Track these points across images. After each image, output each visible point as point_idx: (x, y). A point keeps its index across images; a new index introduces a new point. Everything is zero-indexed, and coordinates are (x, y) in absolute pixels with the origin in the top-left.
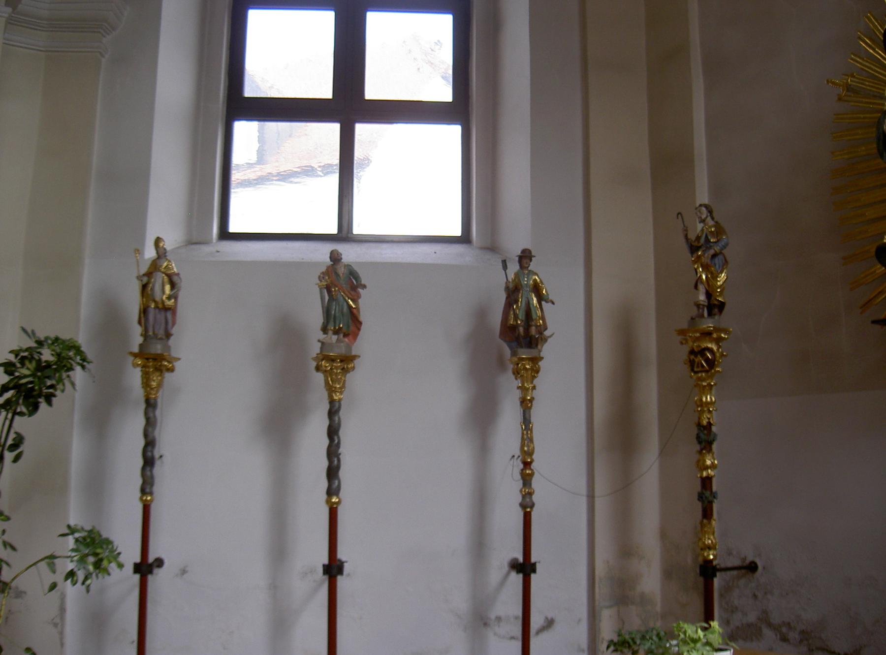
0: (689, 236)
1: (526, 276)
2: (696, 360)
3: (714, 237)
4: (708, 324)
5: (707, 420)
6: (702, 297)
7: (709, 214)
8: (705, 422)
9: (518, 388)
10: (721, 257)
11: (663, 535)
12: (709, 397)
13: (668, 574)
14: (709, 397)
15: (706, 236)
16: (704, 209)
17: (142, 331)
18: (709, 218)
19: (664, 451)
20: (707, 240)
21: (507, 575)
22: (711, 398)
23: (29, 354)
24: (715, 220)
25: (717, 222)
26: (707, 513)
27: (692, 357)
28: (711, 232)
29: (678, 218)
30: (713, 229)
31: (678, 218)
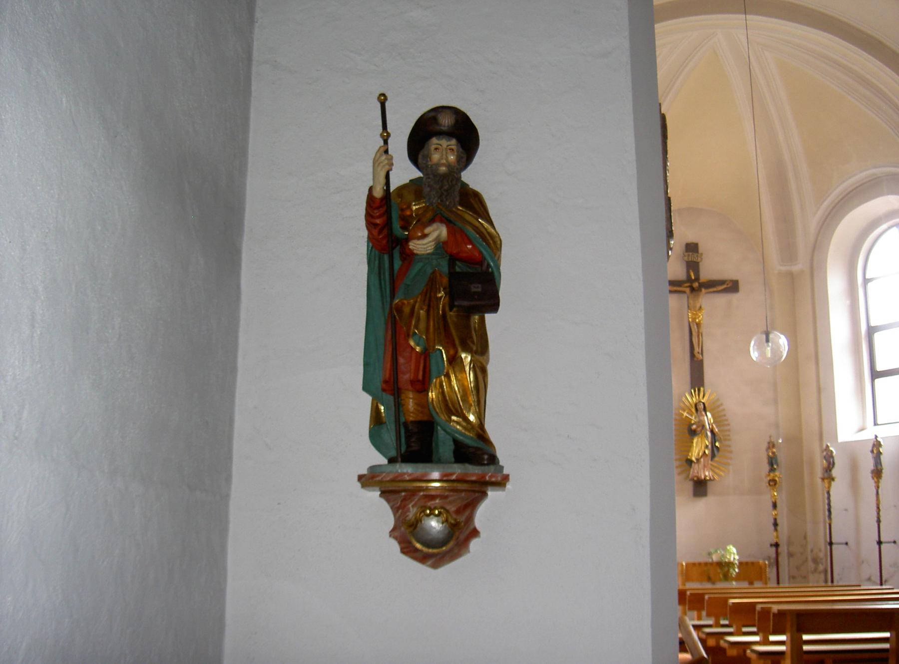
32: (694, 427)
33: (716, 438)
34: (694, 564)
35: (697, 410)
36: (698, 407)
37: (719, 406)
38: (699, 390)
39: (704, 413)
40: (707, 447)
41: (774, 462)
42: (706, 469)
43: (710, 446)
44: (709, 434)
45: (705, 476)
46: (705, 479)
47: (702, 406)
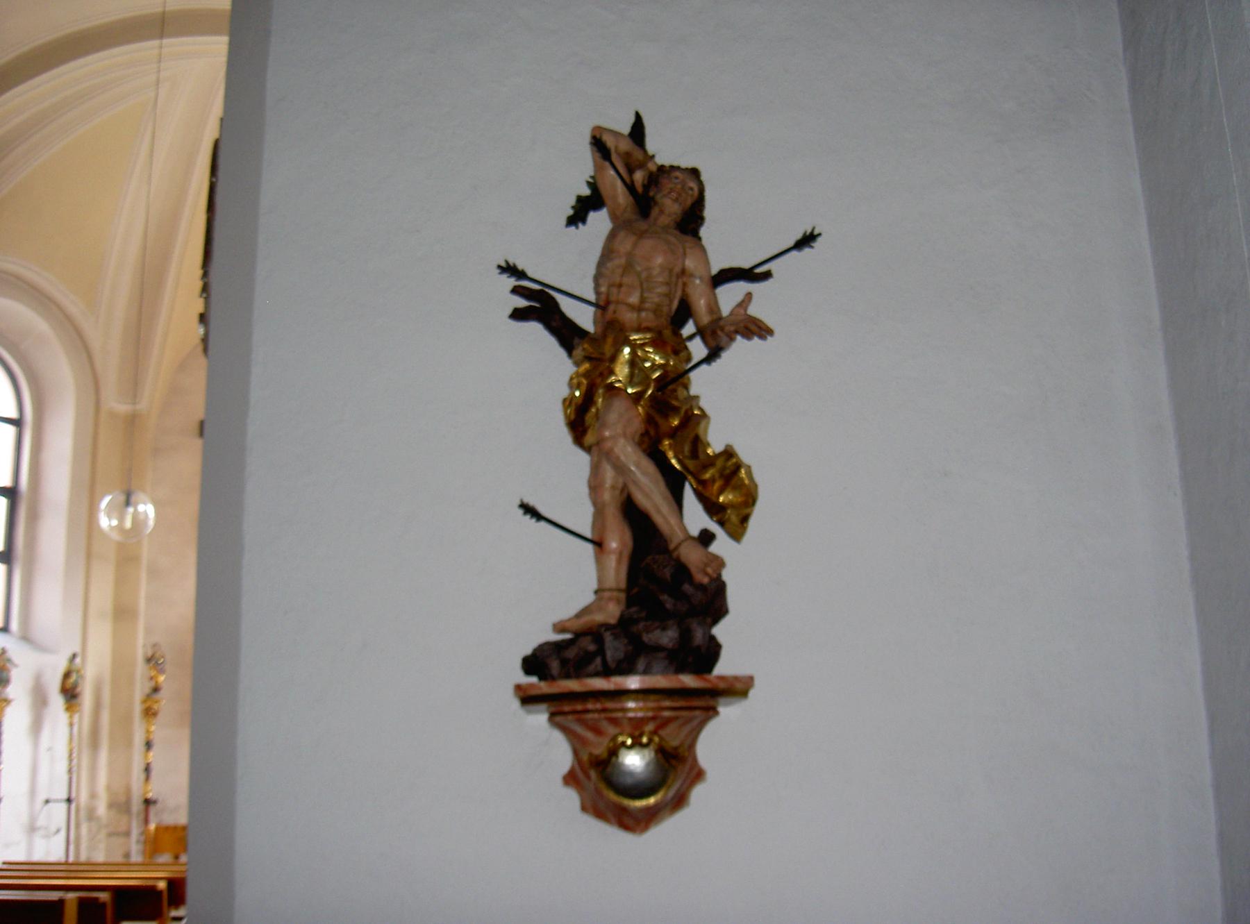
11: (109, 788)
13: (111, 805)
19: (112, 750)
21: (42, 808)
26: (147, 778)
34: (167, 828)
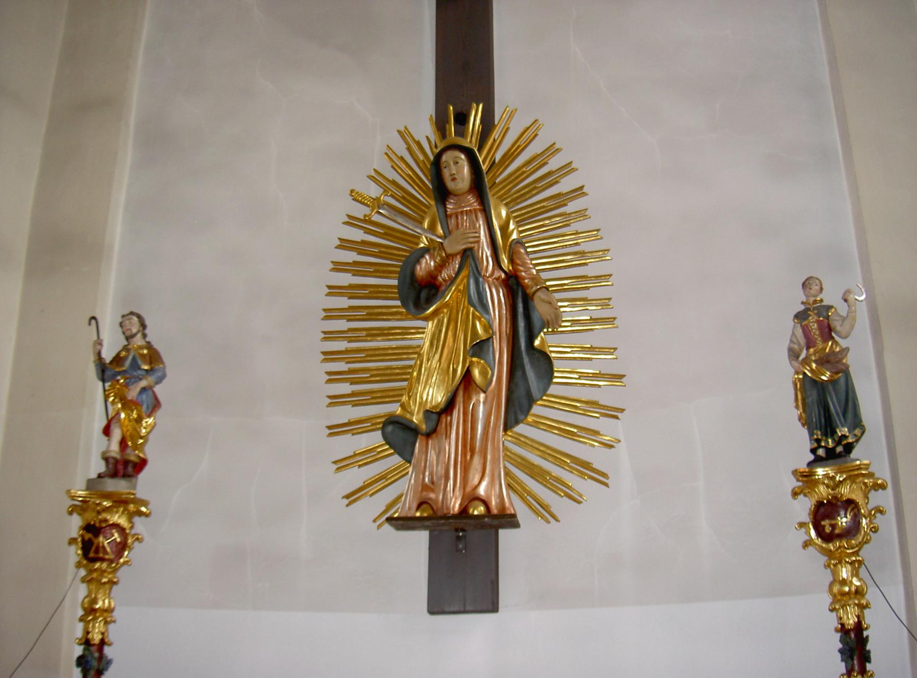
0: (104, 355)
1: (134, 408)
2: (96, 541)
3: (146, 363)
4: (118, 486)
5: (100, 637)
6: (115, 447)
7: (141, 329)
8: (96, 638)
9: (83, 580)
10: (150, 392)
12: (107, 601)
14: (107, 601)
15: (134, 359)
16: (135, 319)
17: (103, 473)
18: (139, 335)
20: (135, 365)
22: (109, 602)
23: (857, 587)
24: (147, 339)
25: (149, 343)
27: (88, 536)
28: (143, 356)
29: (90, 324)
30: (145, 352)
31: (90, 324)
32: (427, 263)
33: (540, 308)
35: (442, 193)
36: (446, 174)
37: (551, 179)
38: (462, 119)
39: (472, 201)
40: (479, 348)
41: (834, 407)
42: (477, 462)
43: (500, 351)
44: (496, 297)
45: (473, 498)
46: (464, 511)
47: (466, 170)
